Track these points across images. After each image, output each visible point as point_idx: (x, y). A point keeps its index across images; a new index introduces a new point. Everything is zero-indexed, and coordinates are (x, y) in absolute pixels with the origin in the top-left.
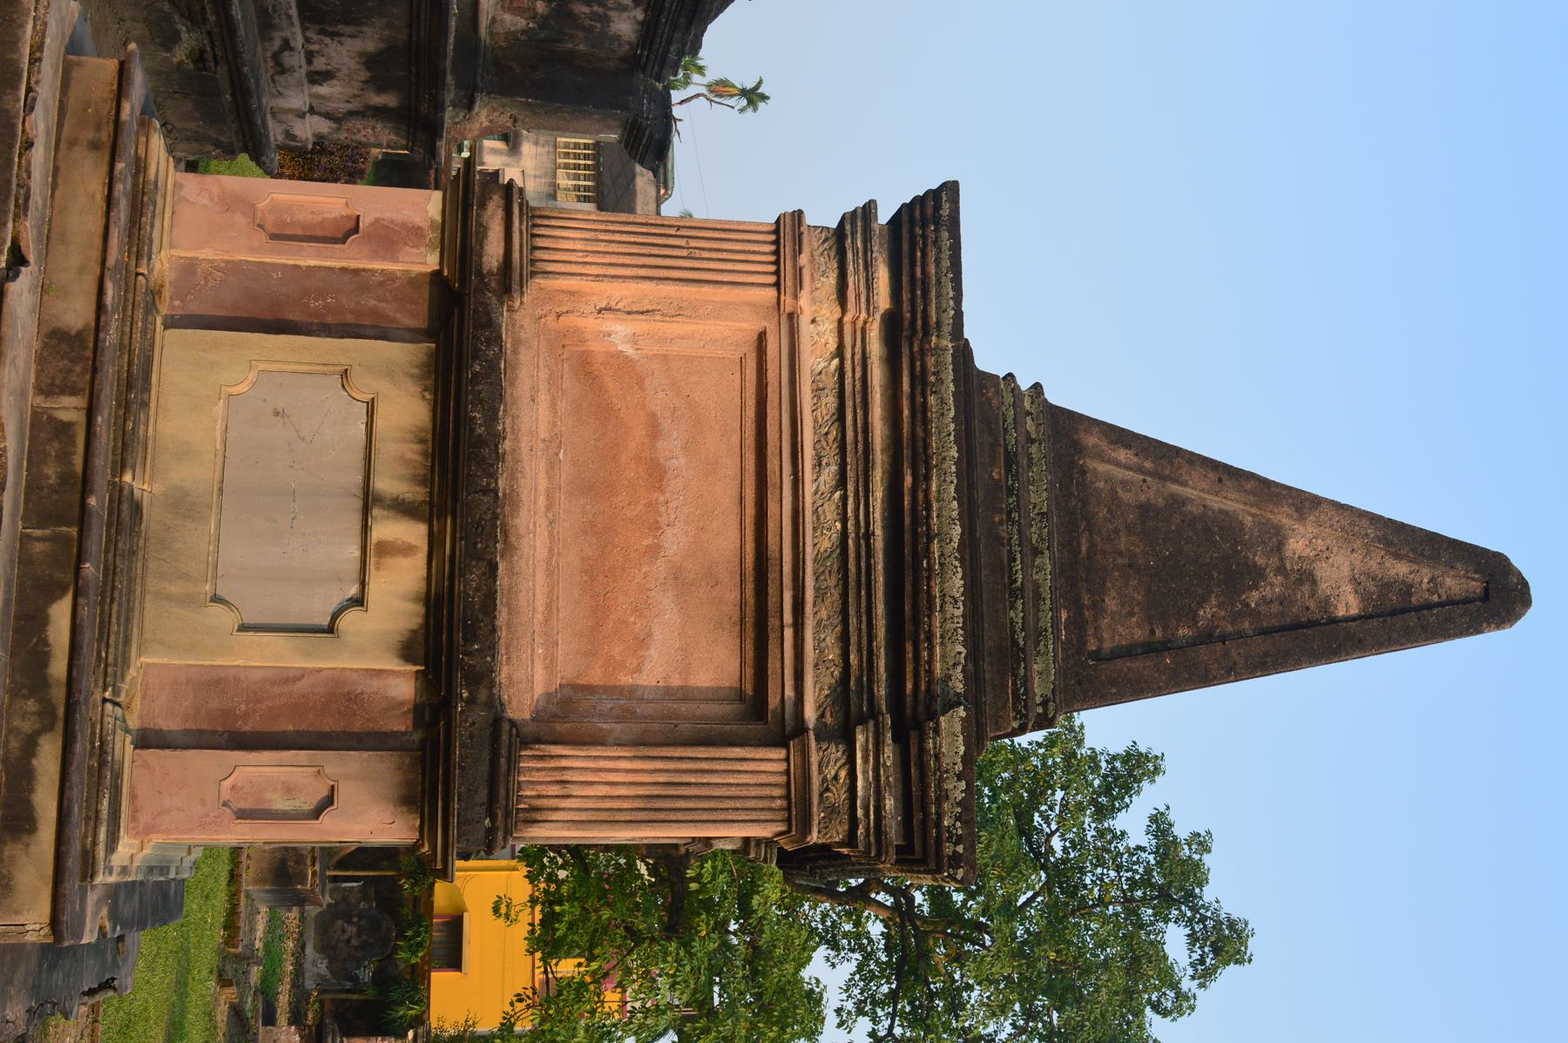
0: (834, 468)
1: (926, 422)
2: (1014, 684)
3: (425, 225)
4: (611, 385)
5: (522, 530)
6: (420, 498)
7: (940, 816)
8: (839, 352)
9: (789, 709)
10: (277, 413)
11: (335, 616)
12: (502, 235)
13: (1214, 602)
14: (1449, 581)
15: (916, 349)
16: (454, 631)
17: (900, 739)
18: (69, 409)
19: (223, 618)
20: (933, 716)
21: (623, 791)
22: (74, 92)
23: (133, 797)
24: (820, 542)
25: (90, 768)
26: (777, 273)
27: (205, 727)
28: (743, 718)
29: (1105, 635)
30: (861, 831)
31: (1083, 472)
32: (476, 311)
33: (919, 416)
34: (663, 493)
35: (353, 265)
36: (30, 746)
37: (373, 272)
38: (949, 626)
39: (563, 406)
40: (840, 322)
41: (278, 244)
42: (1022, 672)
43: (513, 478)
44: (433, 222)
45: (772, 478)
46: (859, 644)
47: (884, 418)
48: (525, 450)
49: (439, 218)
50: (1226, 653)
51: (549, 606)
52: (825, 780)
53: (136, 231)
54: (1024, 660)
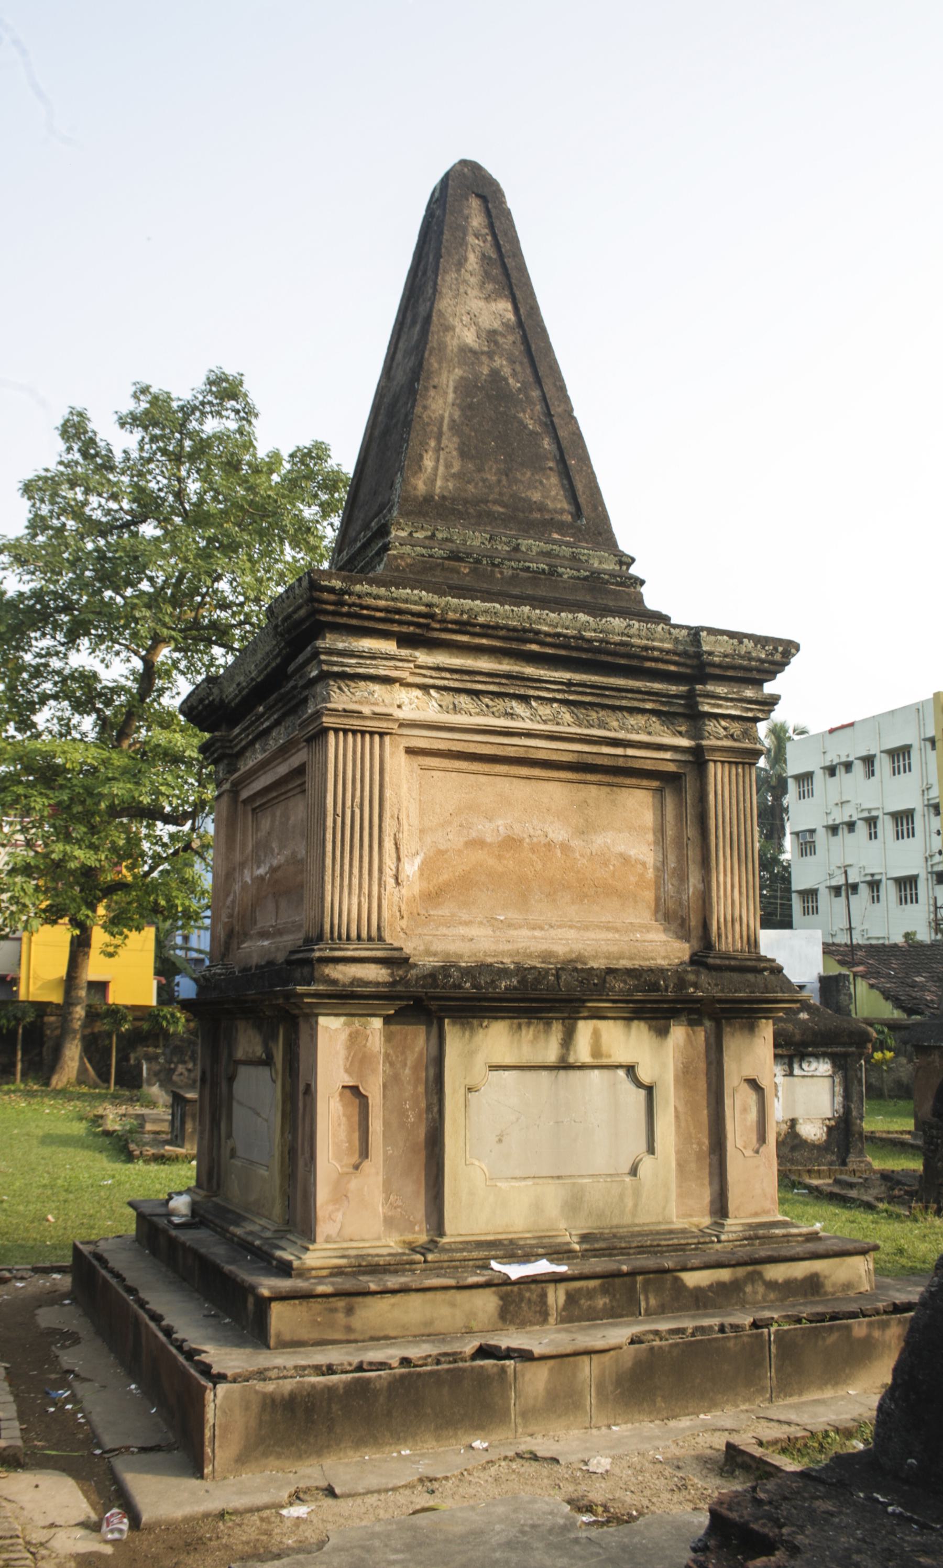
0: (514, 703)
1: (497, 627)
2: (612, 584)
3: (347, 1031)
4: (446, 877)
5: (567, 949)
6: (560, 1027)
8: (425, 688)
9: (678, 757)
10: (500, 1141)
11: (639, 1084)
12: (359, 965)
13: (521, 415)
15: (437, 626)
16: (651, 1000)
19: (647, 1166)
20: (699, 655)
22: (304, 1334)
23: (756, 1214)
24: (567, 722)
25: (760, 1244)
26: (354, 732)
27: (707, 1171)
28: (679, 791)
29: (559, 506)
32: (423, 987)
33: (490, 632)
34: (524, 839)
36: (772, 1285)
38: (643, 634)
39: (465, 917)
42: (606, 577)
43: (530, 956)
44: (345, 1024)
45: (521, 753)
49: (342, 1019)
51: (608, 929)
53: (392, 1268)
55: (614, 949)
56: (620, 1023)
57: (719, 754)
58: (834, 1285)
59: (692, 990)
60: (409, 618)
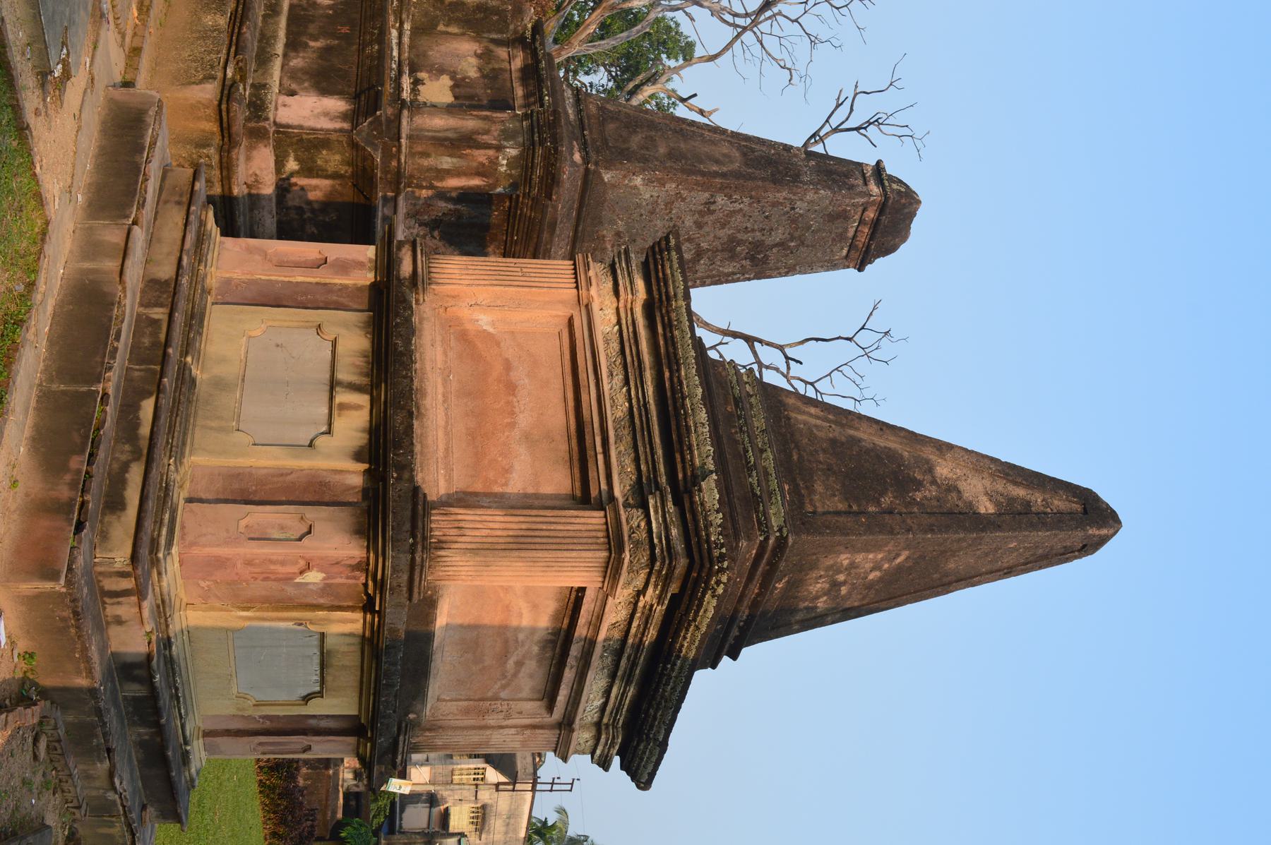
0: (621, 377)
1: (674, 344)
4: (479, 345)
5: (428, 406)
7: (708, 535)
14: (1056, 502)
16: (387, 446)
17: (678, 502)
18: (159, 313)
19: (246, 439)
21: (499, 533)
23: (183, 527)
24: (617, 410)
31: (789, 419)
35: (323, 281)
36: (125, 467)
38: (701, 438)
39: (450, 354)
40: (618, 309)
43: (421, 381)
48: (428, 368)
51: (447, 450)
55: (430, 441)
56: (367, 425)
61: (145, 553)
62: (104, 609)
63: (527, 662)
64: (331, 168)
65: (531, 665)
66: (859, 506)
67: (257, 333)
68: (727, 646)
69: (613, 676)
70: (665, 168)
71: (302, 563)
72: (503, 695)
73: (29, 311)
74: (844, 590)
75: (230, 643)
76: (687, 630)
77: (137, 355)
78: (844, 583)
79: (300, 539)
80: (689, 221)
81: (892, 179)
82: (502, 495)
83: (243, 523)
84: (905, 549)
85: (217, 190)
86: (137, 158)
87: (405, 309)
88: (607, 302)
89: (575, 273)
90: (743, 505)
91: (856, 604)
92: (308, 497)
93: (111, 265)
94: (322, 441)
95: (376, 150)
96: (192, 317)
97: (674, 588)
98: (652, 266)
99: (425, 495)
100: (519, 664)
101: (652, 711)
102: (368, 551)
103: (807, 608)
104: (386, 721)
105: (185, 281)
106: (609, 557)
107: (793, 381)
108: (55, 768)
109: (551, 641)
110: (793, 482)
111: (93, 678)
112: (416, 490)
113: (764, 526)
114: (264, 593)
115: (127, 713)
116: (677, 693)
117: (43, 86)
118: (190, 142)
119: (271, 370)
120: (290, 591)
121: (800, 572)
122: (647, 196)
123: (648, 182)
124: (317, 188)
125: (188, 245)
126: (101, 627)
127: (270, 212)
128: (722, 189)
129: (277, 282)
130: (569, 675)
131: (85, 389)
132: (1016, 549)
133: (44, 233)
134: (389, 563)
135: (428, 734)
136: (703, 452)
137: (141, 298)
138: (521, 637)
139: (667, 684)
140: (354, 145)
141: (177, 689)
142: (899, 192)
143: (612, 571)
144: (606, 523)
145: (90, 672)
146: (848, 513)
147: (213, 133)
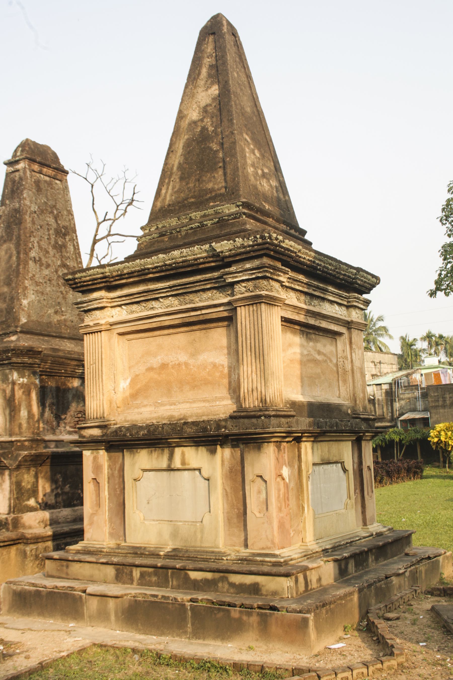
0: (153, 303)
1: (132, 273)
2: (231, 220)
4: (139, 386)
5: (179, 414)
6: (168, 451)
7: (249, 246)
10: (148, 503)
14: (209, 50)
15: (112, 280)
16: (207, 436)
17: (229, 265)
18: (136, 573)
21: (254, 368)
23: (263, 549)
24: (174, 304)
30: (260, 275)
31: (169, 205)
33: (131, 275)
35: (107, 480)
36: (232, 585)
37: (108, 472)
38: (190, 253)
39: (145, 402)
40: (112, 307)
41: (101, 505)
42: (226, 218)
43: (164, 418)
45: (158, 325)
46: (203, 285)
47: (138, 287)
49: (90, 451)
50: (227, 136)
51: (204, 401)
52: (246, 291)
54: (222, 217)
55: (200, 411)
57: (240, 302)
58: (267, 591)
59: (223, 430)
60: (100, 280)
61: (281, 569)
62: (314, 589)
63: (318, 349)
64: (32, 480)
65: (319, 346)
66: (219, 162)
67: (141, 515)
68: (301, 236)
69: (323, 299)
70: (16, 287)
71: (279, 479)
72: (335, 361)
73: (151, 651)
74: (266, 171)
75: (320, 516)
76: (300, 257)
77: (163, 583)
78: (262, 170)
79: (266, 482)
80: (46, 272)
81: (15, 155)
82: (230, 367)
83: (258, 515)
84: (243, 136)
85: (50, 544)
86: (44, 594)
87: (121, 431)
88: (108, 313)
89: (92, 333)
90: (225, 228)
91: (272, 164)
92: (240, 479)
93: (111, 604)
94: (205, 473)
95: (20, 455)
96: (136, 553)
97: (279, 265)
98: (85, 288)
99: (234, 412)
100: (319, 353)
101: (341, 277)
102: (271, 442)
103: (277, 191)
104: (354, 425)
105: (115, 560)
106: (265, 303)
107: (117, 217)
108: (399, 607)
109: (307, 335)
110: (208, 200)
111: (354, 592)
112: (232, 417)
113: (237, 216)
114: (294, 499)
115: (363, 569)
116: (333, 262)
117: (11, 656)
118: (23, 562)
119: (165, 506)
120: (292, 485)
121: (259, 195)
122: (33, 297)
123: (25, 296)
124: (44, 487)
125: (93, 559)
126: (324, 590)
127: (59, 512)
128: (26, 254)
129: (109, 506)
130: (324, 324)
131: (190, 613)
132: (237, 73)
133: (101, 646)
134: (278, 430)
135: (358, 402)
136: (199, 252)
137: (128, 584)
138: (305, 352)
139: (327, 268)
140: (18, 467)
141: (347, 543)
142: (22, 151)
143: (271, 301)
144: (244, 306)
145: (351, 594)
146: (224, 168)
147: (17, 549)
